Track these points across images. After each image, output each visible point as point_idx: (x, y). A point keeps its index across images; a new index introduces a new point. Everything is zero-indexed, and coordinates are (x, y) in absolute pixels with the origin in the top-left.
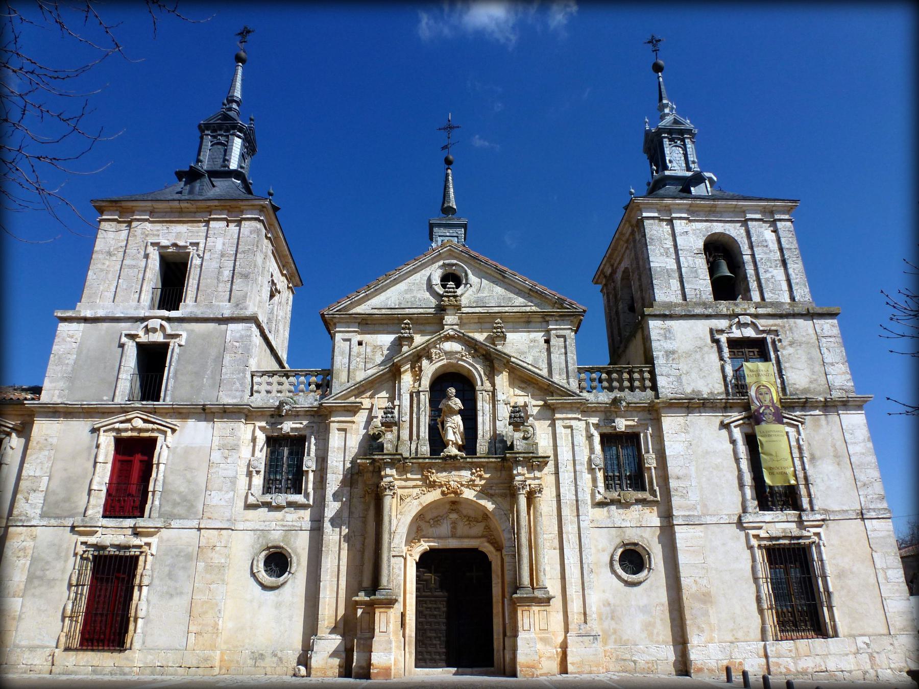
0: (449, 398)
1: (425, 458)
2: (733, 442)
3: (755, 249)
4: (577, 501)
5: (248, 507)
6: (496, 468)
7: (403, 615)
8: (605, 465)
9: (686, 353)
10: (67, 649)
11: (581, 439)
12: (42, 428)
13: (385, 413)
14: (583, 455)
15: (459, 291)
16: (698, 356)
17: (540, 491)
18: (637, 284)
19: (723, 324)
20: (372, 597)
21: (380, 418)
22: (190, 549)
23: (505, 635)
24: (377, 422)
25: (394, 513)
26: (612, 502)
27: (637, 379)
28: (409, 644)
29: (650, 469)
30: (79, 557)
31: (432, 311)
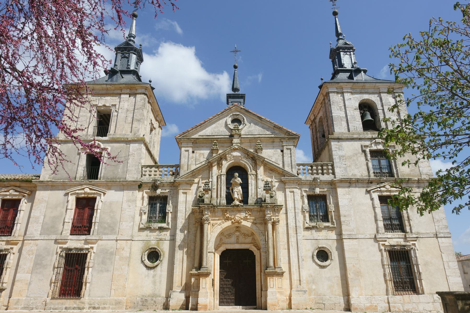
0: (236, 178)
1: (224, 206)
2: (372, 199)
3: (384, 107)
4: (296, 226)
5: (141, 230)
6: (257, 211)
7: (213, 280)
8: (310, 209)
9: (349, 157)
10: (53, 298)
11: (298, 197)
12: (39, 194)
13: (205, 185)
14: (299, 205)
15: (240, 127)
16: (355, 158)
17: (278, 222)
18: (326, 124)
19: (368, 143)
20: (199, 271)
21: (203, 187)
22: (112, 250)
23: (262, 290)
24: (201, 189)
25: (209, 232)
26: (313, 228)
27: (325, 169)
28: (216, 294)
29: (331, 211)
30: (58, 255)
31: (228, 137)
